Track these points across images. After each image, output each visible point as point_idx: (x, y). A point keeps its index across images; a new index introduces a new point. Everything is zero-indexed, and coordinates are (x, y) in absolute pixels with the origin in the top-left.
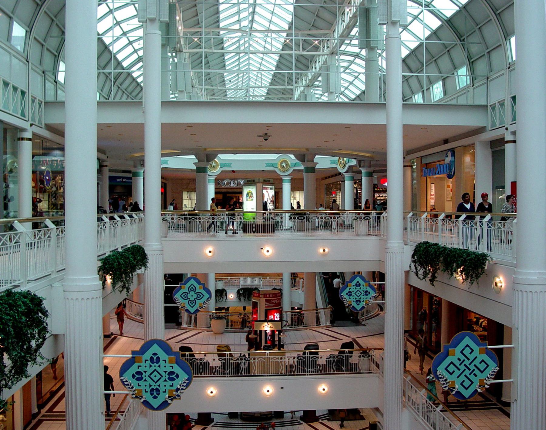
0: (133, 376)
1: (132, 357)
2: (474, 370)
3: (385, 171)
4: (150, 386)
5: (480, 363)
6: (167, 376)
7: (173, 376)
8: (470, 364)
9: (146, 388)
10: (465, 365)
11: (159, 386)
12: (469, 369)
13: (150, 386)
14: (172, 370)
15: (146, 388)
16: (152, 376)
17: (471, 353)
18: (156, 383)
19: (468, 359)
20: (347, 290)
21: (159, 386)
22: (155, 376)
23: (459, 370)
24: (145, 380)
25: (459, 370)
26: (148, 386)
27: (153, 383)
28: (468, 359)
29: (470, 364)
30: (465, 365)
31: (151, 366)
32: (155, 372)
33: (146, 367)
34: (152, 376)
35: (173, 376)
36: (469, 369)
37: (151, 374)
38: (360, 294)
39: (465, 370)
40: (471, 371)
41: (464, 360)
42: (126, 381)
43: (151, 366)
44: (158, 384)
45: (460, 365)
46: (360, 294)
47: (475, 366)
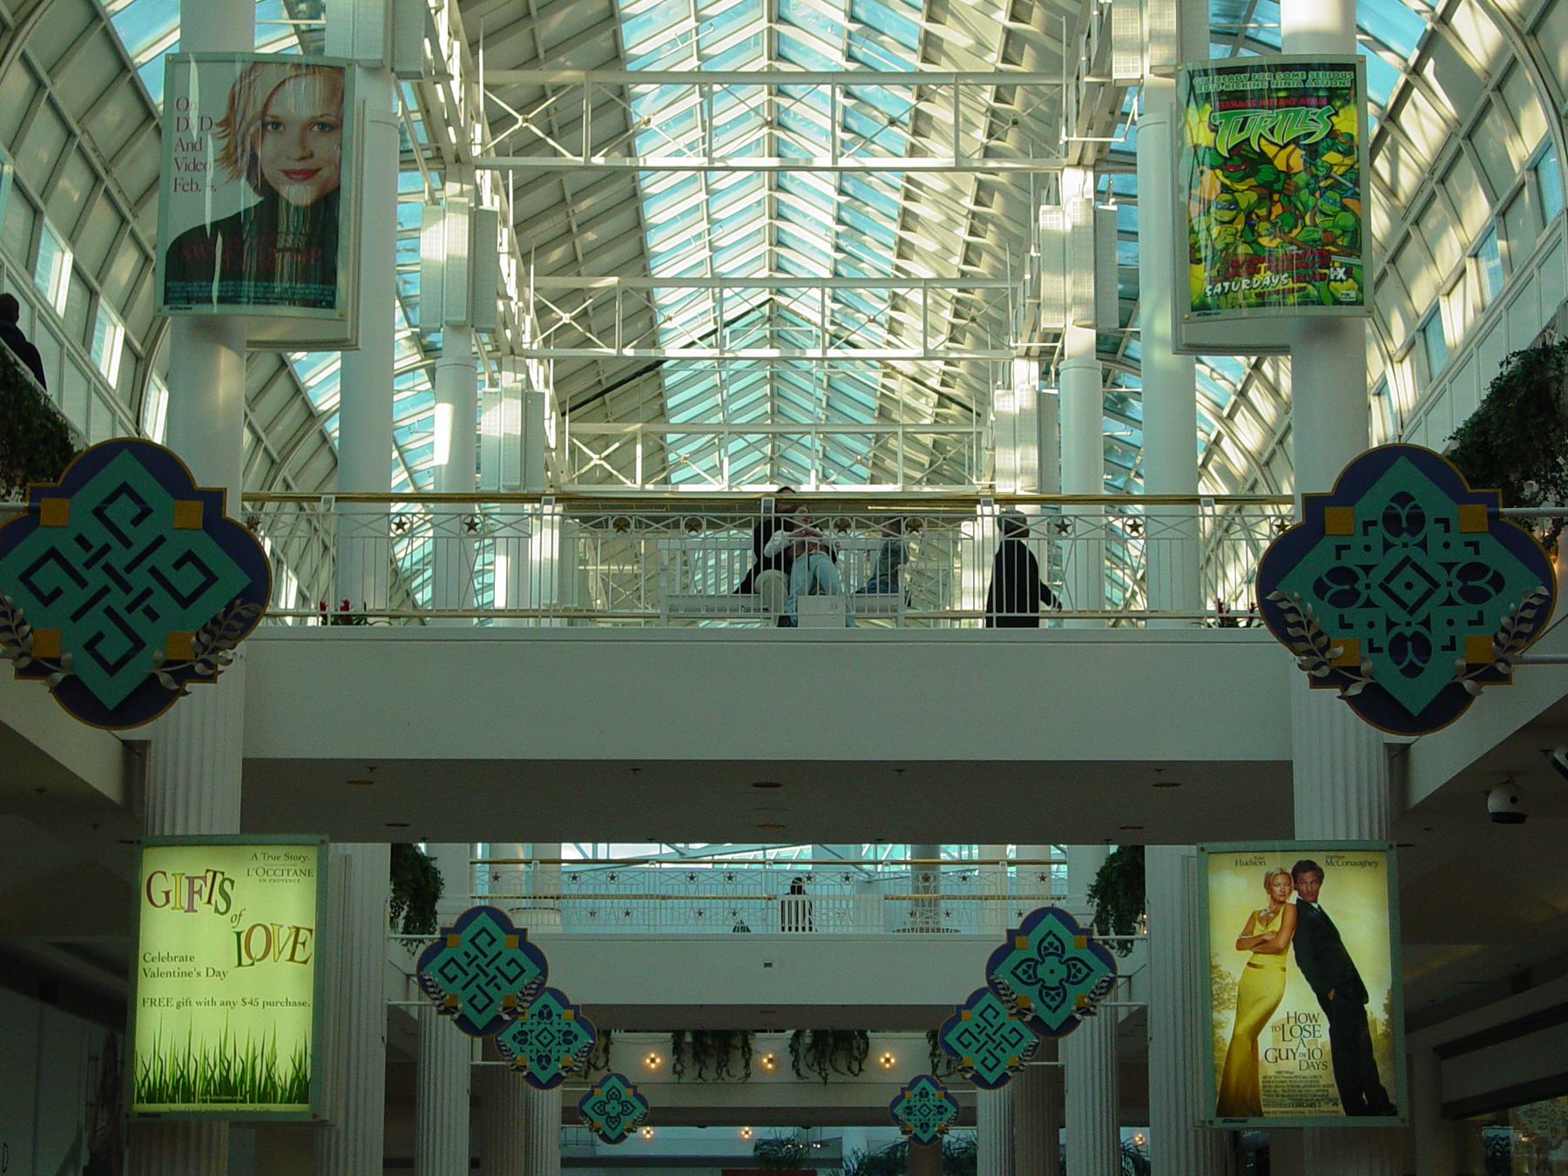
0: (1320, 589)
1: (29, 509)
2: (88, 565)
3: (1145, 1025)
4: (1390, 625)
5: (57, 592)
6: (1458, 584)
7: (1482, 583)
8: (106, 590)
9: (1371, 633)
10: (127, 589)
11: (1426, 623)
12: (108, 569)
13: (1390, 625)
14: (1477, 559)
15: (1371, 633)
16: (1396, 586)
17: (99, 636)
18: (1412, 612)
19: (109, 611)
20: (515, 1028)
21: (1426, 623)
22: (1409, 586)
23: (154, 571)
24: (1369, 603)
25: (154, 571)
26: (1381, 624)
27: (1399, 615)
28: (109, 611)
29: (106, 590)
30: (127, 589)
31: (1387, 546)
32: (1408, 569)
33: (1367, 548)
34: (1396, 586)
35: (1482, 583)
36: (108, 569)
37: (1390, 578)
38: (1421, 586)
39: (129, 569)
40: (102, 562)
41: (130, 608)
42: (1292, 610)
43: (1387, 546)
44: (1421, 614)
45: (148, 592)
46: (1421, 586)
47: (82, 583)
